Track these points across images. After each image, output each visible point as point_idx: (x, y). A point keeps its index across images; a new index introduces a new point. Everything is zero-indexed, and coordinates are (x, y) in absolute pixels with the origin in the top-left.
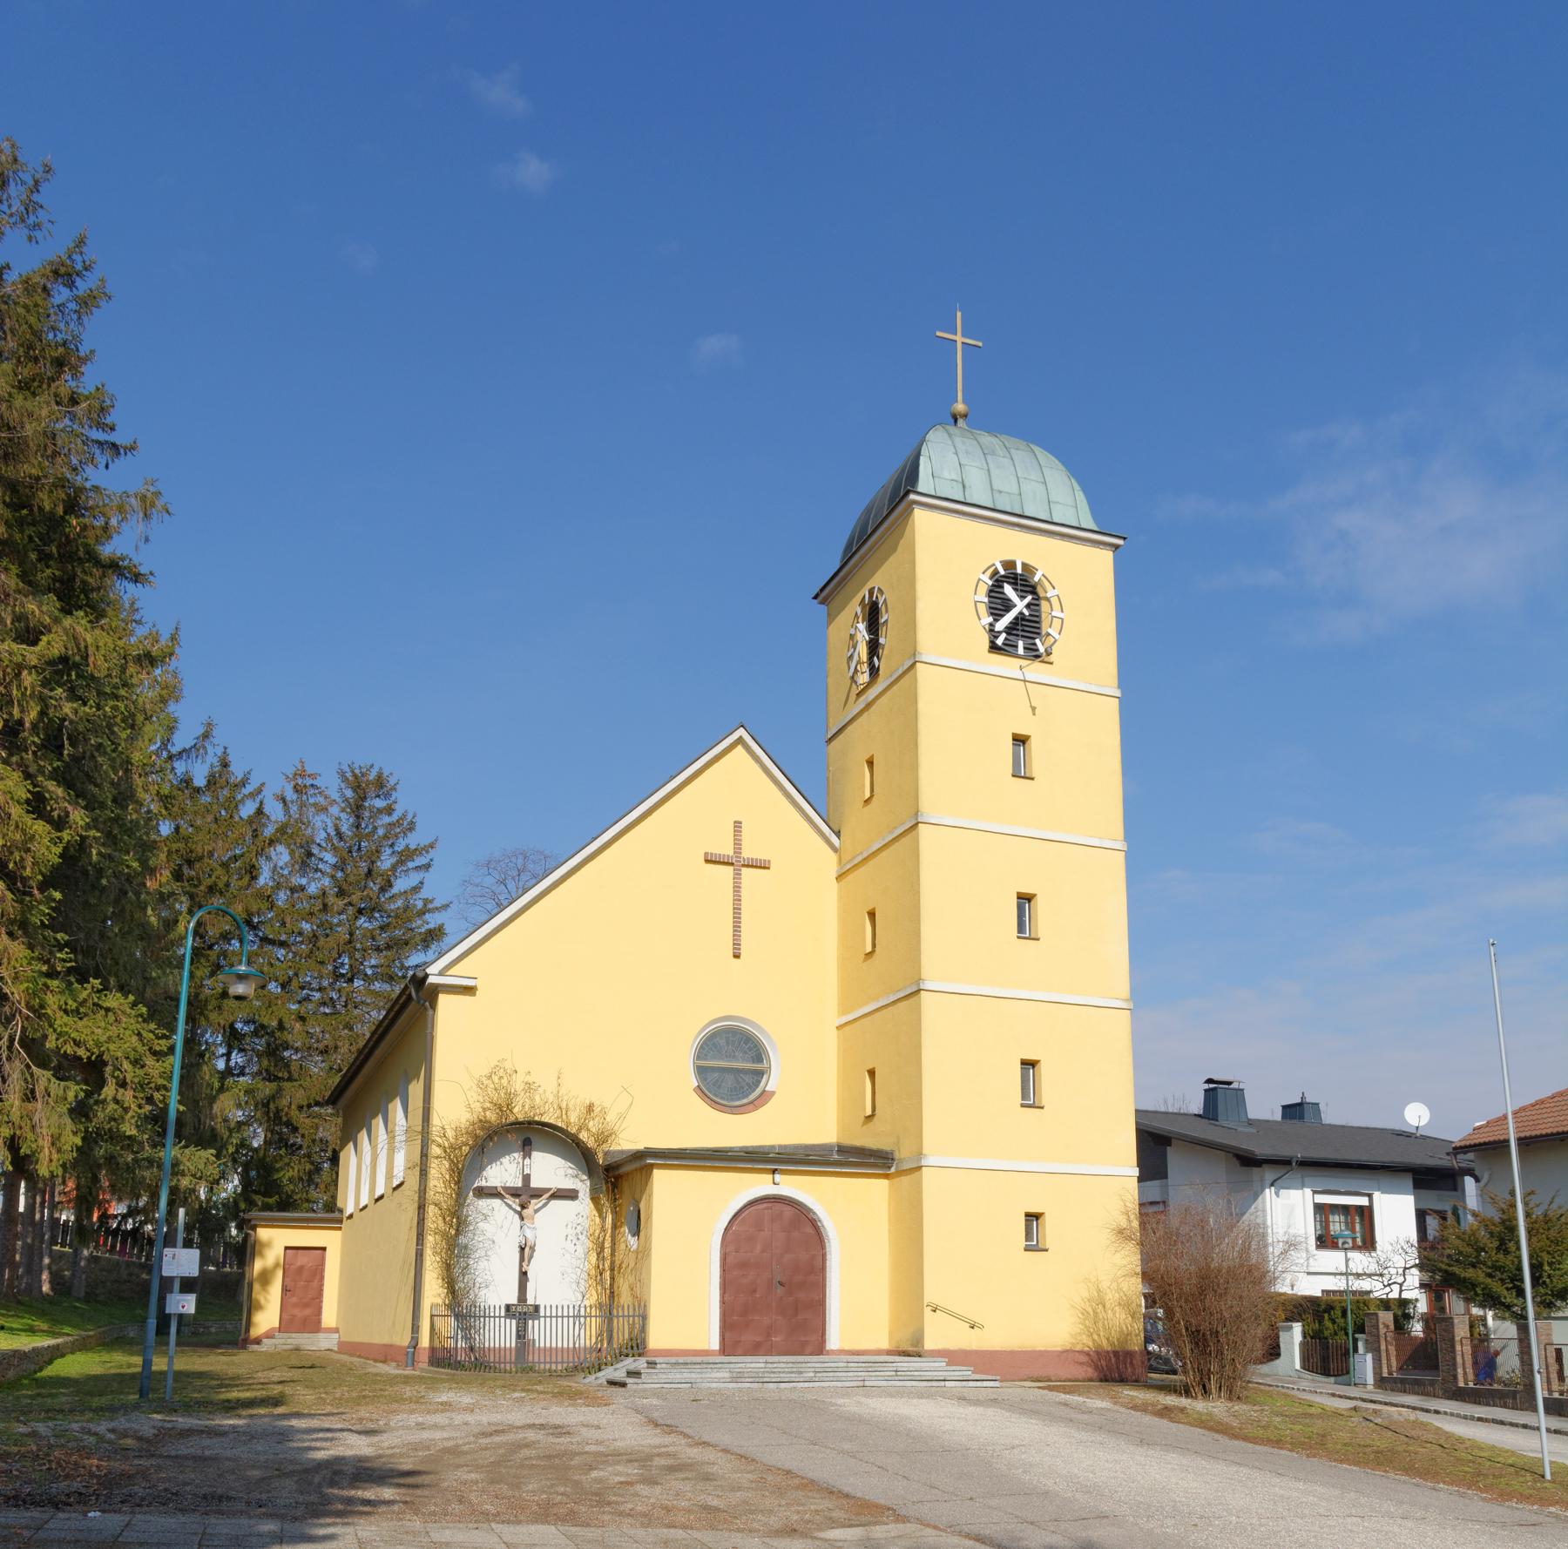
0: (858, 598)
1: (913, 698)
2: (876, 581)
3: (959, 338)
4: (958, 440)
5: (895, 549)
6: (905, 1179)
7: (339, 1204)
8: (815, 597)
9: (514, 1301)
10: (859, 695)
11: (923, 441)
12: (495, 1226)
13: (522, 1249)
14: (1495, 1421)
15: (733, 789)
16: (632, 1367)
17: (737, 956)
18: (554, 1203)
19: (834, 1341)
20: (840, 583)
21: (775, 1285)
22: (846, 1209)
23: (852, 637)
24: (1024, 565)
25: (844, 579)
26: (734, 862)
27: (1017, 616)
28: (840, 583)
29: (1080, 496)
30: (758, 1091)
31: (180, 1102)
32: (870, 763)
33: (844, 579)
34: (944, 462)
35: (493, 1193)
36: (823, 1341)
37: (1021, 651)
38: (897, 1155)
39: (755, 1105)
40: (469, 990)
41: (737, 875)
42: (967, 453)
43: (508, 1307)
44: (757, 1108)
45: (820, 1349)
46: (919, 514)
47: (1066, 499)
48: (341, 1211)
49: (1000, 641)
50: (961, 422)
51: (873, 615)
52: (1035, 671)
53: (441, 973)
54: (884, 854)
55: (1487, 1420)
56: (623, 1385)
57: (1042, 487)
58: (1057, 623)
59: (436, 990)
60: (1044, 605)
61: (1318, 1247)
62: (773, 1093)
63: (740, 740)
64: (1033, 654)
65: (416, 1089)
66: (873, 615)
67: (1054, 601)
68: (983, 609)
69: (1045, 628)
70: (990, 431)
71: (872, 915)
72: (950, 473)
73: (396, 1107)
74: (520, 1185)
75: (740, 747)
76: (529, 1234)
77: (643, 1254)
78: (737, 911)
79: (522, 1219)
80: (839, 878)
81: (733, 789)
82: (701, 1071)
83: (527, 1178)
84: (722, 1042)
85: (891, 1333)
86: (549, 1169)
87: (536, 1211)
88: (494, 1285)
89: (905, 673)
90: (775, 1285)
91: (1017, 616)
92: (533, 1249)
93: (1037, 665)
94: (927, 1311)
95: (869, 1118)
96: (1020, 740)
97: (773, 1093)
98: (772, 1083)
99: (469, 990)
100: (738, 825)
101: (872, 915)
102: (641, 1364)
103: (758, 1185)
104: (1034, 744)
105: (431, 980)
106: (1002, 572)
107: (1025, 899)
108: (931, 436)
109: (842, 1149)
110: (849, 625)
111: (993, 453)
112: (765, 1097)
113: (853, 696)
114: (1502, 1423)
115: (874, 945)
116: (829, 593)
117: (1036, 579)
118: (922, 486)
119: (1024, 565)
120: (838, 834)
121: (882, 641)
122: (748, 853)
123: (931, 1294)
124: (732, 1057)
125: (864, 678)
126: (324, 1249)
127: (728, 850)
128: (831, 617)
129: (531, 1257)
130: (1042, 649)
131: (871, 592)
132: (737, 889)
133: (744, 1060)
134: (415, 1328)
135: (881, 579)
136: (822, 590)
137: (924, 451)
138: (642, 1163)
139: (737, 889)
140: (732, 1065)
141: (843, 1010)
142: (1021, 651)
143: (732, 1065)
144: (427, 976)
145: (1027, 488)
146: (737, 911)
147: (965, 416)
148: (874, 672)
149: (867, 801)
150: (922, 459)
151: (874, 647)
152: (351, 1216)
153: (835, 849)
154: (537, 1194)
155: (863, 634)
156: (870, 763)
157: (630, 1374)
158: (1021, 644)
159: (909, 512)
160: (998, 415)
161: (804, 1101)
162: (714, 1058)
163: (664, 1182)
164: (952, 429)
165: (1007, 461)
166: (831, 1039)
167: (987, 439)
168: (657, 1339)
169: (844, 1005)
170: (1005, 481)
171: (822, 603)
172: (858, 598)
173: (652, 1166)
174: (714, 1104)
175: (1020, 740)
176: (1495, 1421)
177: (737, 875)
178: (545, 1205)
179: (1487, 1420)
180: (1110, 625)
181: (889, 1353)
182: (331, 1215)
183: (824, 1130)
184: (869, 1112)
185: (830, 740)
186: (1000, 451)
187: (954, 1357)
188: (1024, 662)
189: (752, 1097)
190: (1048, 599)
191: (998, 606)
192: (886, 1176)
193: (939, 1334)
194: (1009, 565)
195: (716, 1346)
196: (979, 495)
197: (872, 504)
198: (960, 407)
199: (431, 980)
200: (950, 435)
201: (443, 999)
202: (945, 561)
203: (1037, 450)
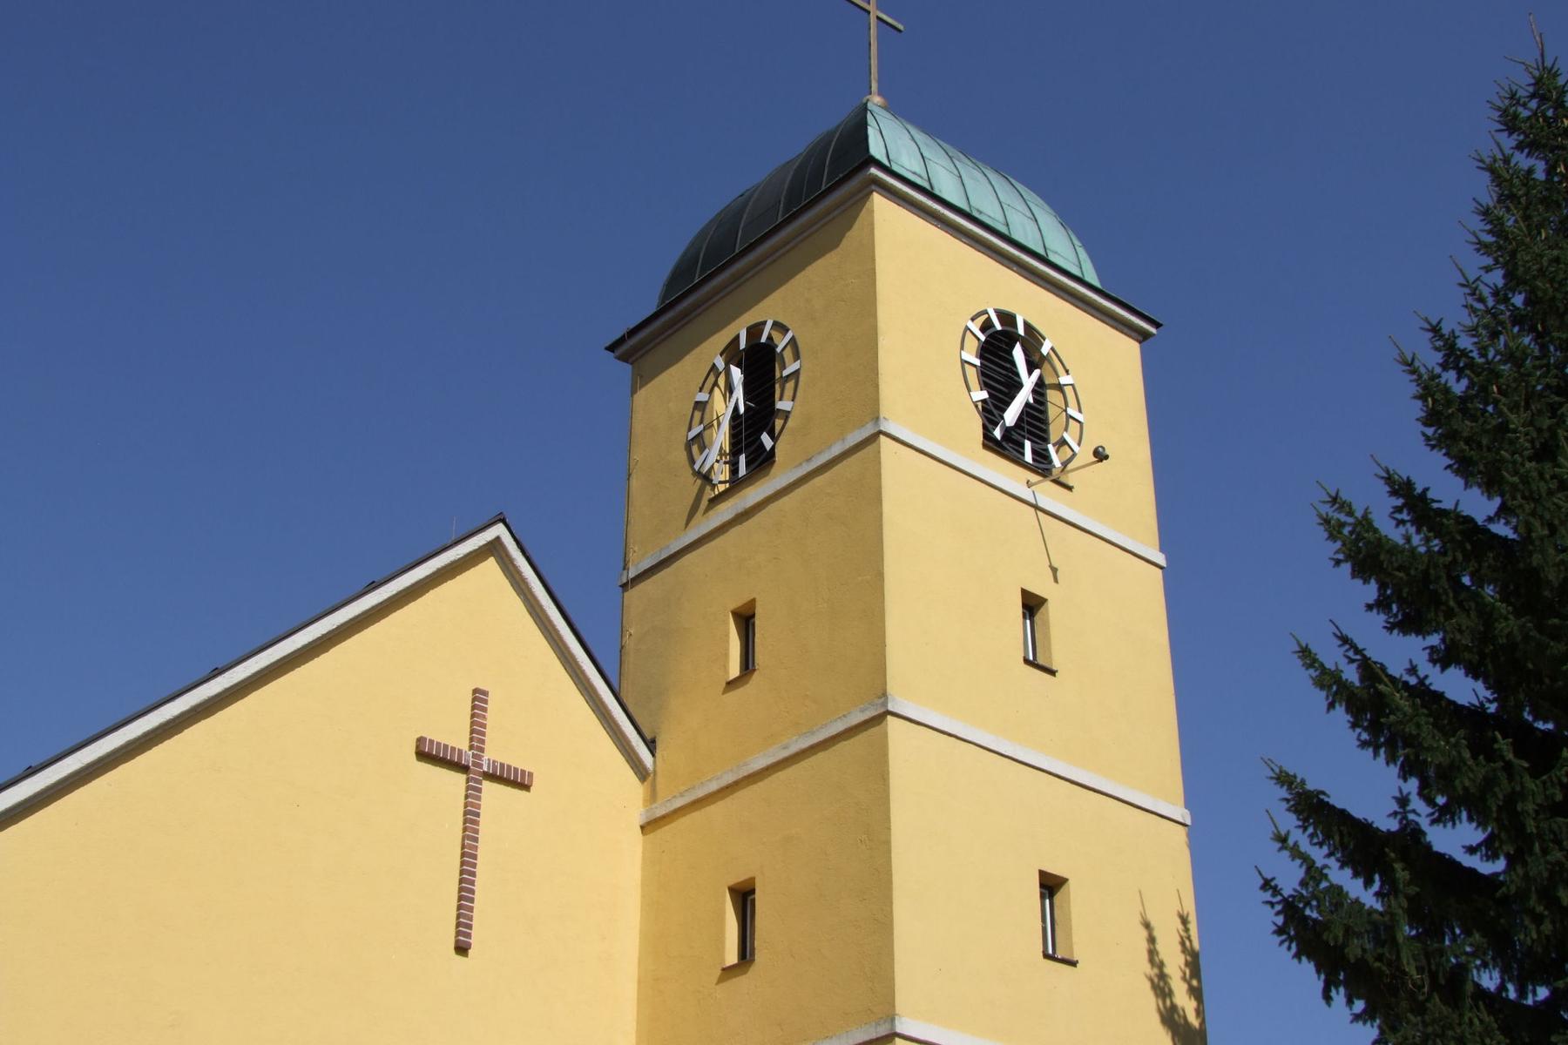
0: (722, 339)
2: (767, 311)
5: (834, 244)
8: (611, 348)
10: (715, 501)
15: (470, 636)
20: (672, 324)
23: (700, 406)
25: (685, 314)
28: (672, 324)
31: (1368, 883)
32: (746, 620)
33: (685, 314)
37: (1028, 457)
41: (472, 793)
51: (760, 364)
52: (1047, 494)
54: (781, 775)
57: (1033, 224)
60: (1053, 396)
63: (495, 548)
64: (1042, 466)
66: (760, 364)
75: (491, 563)
78: (468, 859)
81: (470, 636)
93: (1048, 485)
100: (479, 698)
101: (744, 897)
104: (1054, 612)
106: (999, 327)
110: (697, 391)
113: (704, 503)
116: (643, 347)
117: (1045, 350)
120: (651, 745)
122: (496, 752)
127: (456, 738)
128: (641, 379)
130: (1057, 462)
131: (754, 331)
132: (471, 817)
135: (786, 307)
136: (633, 332)
139: (471, 817)
146: (468, 859)
150: (872, 132)
153: (642, 773)
155: (727, 403)
156: (746, 620)
171: (624, 358)
172: (722, 339)
175: (1032, 605)
177: (472, 793)
185: (625, 587)
188: (1034, 478)
197: (830, 135)
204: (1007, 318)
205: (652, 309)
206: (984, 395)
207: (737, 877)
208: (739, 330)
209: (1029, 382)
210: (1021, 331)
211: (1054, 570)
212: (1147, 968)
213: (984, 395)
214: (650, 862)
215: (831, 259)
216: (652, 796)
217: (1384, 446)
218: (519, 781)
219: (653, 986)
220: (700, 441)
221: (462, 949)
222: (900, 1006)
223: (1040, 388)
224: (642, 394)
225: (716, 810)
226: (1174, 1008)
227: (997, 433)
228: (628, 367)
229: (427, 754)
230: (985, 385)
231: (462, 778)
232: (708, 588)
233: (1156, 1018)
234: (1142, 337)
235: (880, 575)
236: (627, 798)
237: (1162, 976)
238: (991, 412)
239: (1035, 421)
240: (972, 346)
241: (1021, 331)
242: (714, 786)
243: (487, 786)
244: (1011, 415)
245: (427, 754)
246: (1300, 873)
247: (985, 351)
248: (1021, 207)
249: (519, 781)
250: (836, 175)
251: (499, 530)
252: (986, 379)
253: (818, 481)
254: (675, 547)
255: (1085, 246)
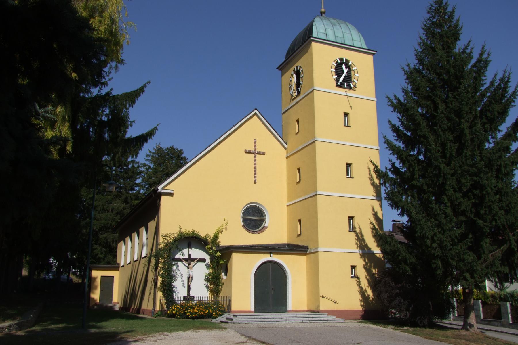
0: (292, 69)
1: (312, 101)
2: (299, 63)
4: (324, 21)
6: (312, 255)
7: (118, 262)
8: (278, 68)
9: (186, 295)
10: (293, 99)
11: (313, 21)
12: (181, 270)
13: (189, 278)
14: (496, 331)
16: (228, 317)
17: (255, 183)
18: (199, 264)
19: (290, 307)
21: (271, 288)
22: (294, 266)
23: (291, 81)
24: (346, 60)
25: (288, 63)
26: (253, 153)
27: (344, 74)
29: (362, 38)
30: (262, 226)
32: (298, 121)
33: (288, 63)
34: (320, 28)
35: (179, 260)
36: (286, 308)
37: (346, 86)
38: (309, 247)
39: (261, 231)
40: (171, 195)
41: (255, 157)
42: (327, 25)
43: (185, 297)
44: (262, 232)
45: (286, 311)
46: (313, 43)
47: (359, 41)
48: (119, 264)
50: (323, 15)
51: (298, 73)
52: (350, 93)
53: (163, 189)
54: (303, 150)
55: (493, 331)
56: (227, 323)
58: (356, 78)
59: (161, 194)
60: (352, 72)
62: (267, 227)
63: (255, 114)
64: (349, 87)
65: (152, 225)
66: (298, 73)
67: (356, 71)
68: (334, 73)
69: (353, 79)
70: (334, 18)
71: (299, 170)
72: (322, 31)
73: (143, 230)
76: (191, 273)
77: (230, 280)
78: (255, 168)
79: (188, 268)
80: (287, 158)
81: (254, 130)
82: (244, 220)
83: (190, 255)
84: (251, 211)
85: (308, 305)
86: (197, 253)
87: (193, 266)
88: (180, 292)
89: (310, 93)
90: (271, 288)
91: (344, 74)
92: (192, 278)
93: (351, 91)
94: (321, 298)
95: (299, 235)
96: (346, 115)
97: (267, 227)
98: (267, 224)
99: (171, 195)
100: (255, 141)
101: (299, 170)
102: (231, 316)
103: (265, 258)
104: (350, 116)
106: (339, 62)
107: (349, 165)
108: (316, 19)
109: (289, 245)
111: (335, 25)
112: (265, 228)
114: (498, 332)
115: (300, 180)
116: (283, 68)
117: (350, 64)
118: (315, 34)
120: (286, 143)
121: (301, 83)
122: (258, 150)
123: (322, 292)
124: (253, 215)
125: (295, 94)
126: (113, 277)
127: (252, 149)
128: (283, 74)
129: (191, 281)
130: (352, 86)
131: (297, 67)
132: (255, 161)
133: (257, 216)
134: (154, 304)
135: (301, 63)
137: (314, 24)
138: (228, 251)
139: (255, 161)
140: (254, 218)
141: (289, 200)
142: (346, 86)
143: (254, 218)
145: (346, 35)
146: (255, 168)
147: (324, 13)
148: (299, 93)
149: (297, 134)
150: (314, 27)
151: (298, 85)
152: (123, 266)
153: (285, 148)
154: (193, 260)
155: (294, 81)
156: (298, 121)
157: (228, 319)
158: (346, 84)
159: (310, 44)
160: (337, 13)
161: (277, 229)
162: (248, 216)
163: (236, 258)
164: (322, 17)
165: (339, 27)
166: (285, 210)
167: (333, 21)
168: (234, 308)
169: (289, 198)
171: (280, 70)
174: (248, 231)
175: (346, 115)
176: (496, 331)
177: (255, 157)
178: (196, 264)
179: (493, 331)
180: (372, 78)
181: (307, 311)
182: (116, 268)
183: (283, 239)
184: (299, 233)
186: (337, 24)
187: (330, 313)
188: (347, 90)
189: (260, 228)
190: (353, 70)
191: (339, 71)
192: (305, 255)
193: (325, 305)
195: (253, 309)
196: (331, 37)
198: (323, 10)
199: (159, 191)
200: (321, 19)
201: (163, 198)
202: (322, 59)
203: (348, 24)
204: (341, 59)
205: (283, 59)
206: (336, 76)
207: (298, 167)
208: (295, 67)
209: (346, 71)
210: (344, 61)
211: (351, 107)
212: (368, 176)
213: (336, 76)
214: (288, 164)
215: (307, 54)
216: (287, 152)
217: (399, 86)
218: (263, 154)
219: (289, 184)
220: (290, 88)
221: (255, 183)
222: (318, 190)
223: (349, 72)
224: (283, 77)
225: (295, 155)
226: (374, 182)
227: (339, 83)
228: (280, 72)
229: (247, 152)
230: (336, 75)
231: (253, 155)
232: (293, 115)
233: (370, 184)
234: (373, 54)
235: (314, 116)
236: (283, 153)
237: (372, 177)
238: (337, 80)
239: (348, 79)
240: (334, 67)
241: (344, 61)
242: (295, 151)
243: (257, 155)
244: (341, 80)
245: (247, 152)
246: (374, 167)
247: (336, 68)
248: (348, 32)
249: (263, 154)
250: (304, 40)
251: (256, 111)
252: (336, 73)
253: (306, 98)
254: (288, 108)
255: (363, 36)
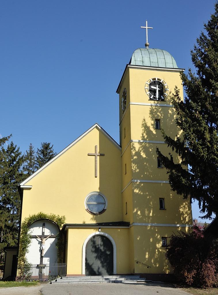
3: (147, 27)
20: (120, 88)
29: (174, 61)
44: (102, 213)
49: (152, 97)
50: (147, 47)
61: (13, 255)
62: (106, 209)
74: (41, 235)
82: (88, 205)
97: (106, 209)
99: (30, 189)
105: (21, 187)
119: (158, 79)
144: (20, 186)
170: (154, 58)
173: (68, 228)
194: (154, 79)
196: (147, 63)
199: (21, 187)
